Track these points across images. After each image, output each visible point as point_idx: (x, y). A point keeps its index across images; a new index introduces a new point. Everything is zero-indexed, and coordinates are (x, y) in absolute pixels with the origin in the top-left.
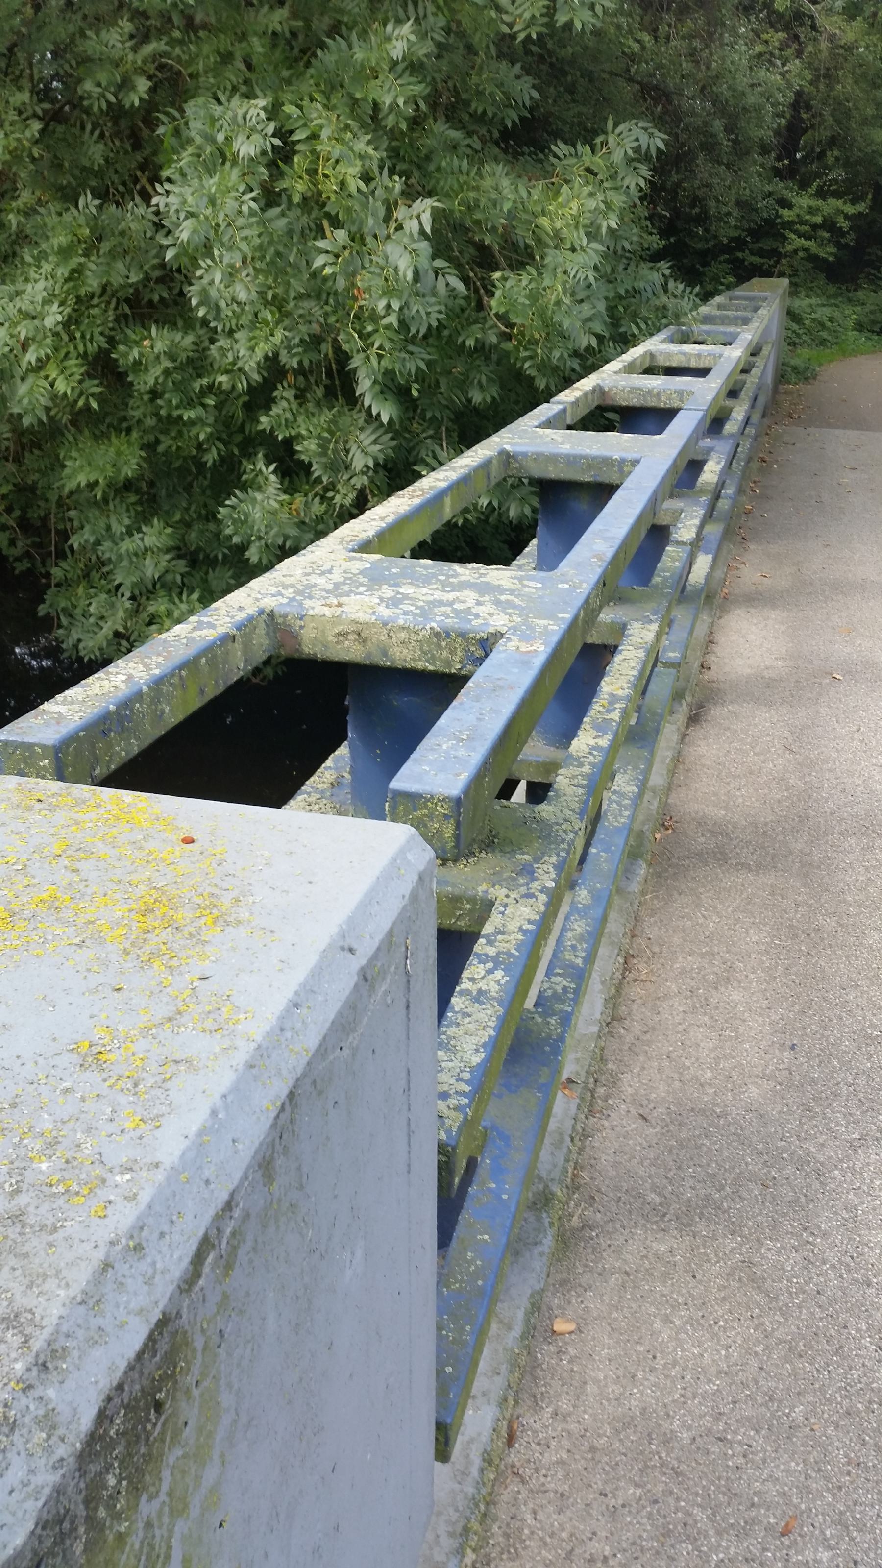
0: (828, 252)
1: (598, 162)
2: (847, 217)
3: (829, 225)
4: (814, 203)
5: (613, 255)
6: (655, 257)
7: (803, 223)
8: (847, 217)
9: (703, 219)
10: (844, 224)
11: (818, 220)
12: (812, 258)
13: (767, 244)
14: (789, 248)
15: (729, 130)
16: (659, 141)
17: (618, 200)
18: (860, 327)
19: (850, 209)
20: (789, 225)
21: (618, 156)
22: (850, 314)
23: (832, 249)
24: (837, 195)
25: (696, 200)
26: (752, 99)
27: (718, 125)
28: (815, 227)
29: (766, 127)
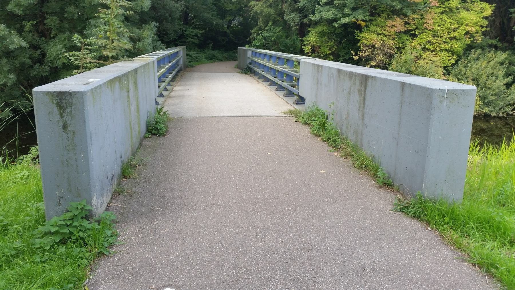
0: (197, 41)
1: (149, 27)
2: (200, 34)
3: (196, 35)
4: (192, 30)
5: (153, 40)
6: (159, 40)
7: (191, 35)
8: (200, 34)
9: (166, 34)
10: (200, 35)
11: (193, 34)
12: (193, 43)
13: (183, 40)
14: (188, 41)
15: (170, 16)
16: (158, 24)
17: (153, 32)
18: (206, 58)
19: (201, 32)
20: (187, 35)
21: (152, 27)
22: (204, 55)
23: (197, 41)
24: (197, 28)
25: (164, 30)
26: (174, 10)
27: (167, 15)
28: (193, 36)
29: (177, 15)
